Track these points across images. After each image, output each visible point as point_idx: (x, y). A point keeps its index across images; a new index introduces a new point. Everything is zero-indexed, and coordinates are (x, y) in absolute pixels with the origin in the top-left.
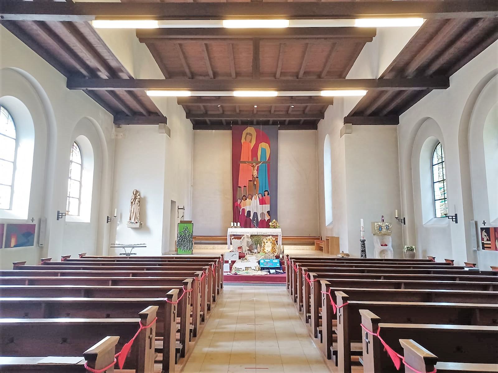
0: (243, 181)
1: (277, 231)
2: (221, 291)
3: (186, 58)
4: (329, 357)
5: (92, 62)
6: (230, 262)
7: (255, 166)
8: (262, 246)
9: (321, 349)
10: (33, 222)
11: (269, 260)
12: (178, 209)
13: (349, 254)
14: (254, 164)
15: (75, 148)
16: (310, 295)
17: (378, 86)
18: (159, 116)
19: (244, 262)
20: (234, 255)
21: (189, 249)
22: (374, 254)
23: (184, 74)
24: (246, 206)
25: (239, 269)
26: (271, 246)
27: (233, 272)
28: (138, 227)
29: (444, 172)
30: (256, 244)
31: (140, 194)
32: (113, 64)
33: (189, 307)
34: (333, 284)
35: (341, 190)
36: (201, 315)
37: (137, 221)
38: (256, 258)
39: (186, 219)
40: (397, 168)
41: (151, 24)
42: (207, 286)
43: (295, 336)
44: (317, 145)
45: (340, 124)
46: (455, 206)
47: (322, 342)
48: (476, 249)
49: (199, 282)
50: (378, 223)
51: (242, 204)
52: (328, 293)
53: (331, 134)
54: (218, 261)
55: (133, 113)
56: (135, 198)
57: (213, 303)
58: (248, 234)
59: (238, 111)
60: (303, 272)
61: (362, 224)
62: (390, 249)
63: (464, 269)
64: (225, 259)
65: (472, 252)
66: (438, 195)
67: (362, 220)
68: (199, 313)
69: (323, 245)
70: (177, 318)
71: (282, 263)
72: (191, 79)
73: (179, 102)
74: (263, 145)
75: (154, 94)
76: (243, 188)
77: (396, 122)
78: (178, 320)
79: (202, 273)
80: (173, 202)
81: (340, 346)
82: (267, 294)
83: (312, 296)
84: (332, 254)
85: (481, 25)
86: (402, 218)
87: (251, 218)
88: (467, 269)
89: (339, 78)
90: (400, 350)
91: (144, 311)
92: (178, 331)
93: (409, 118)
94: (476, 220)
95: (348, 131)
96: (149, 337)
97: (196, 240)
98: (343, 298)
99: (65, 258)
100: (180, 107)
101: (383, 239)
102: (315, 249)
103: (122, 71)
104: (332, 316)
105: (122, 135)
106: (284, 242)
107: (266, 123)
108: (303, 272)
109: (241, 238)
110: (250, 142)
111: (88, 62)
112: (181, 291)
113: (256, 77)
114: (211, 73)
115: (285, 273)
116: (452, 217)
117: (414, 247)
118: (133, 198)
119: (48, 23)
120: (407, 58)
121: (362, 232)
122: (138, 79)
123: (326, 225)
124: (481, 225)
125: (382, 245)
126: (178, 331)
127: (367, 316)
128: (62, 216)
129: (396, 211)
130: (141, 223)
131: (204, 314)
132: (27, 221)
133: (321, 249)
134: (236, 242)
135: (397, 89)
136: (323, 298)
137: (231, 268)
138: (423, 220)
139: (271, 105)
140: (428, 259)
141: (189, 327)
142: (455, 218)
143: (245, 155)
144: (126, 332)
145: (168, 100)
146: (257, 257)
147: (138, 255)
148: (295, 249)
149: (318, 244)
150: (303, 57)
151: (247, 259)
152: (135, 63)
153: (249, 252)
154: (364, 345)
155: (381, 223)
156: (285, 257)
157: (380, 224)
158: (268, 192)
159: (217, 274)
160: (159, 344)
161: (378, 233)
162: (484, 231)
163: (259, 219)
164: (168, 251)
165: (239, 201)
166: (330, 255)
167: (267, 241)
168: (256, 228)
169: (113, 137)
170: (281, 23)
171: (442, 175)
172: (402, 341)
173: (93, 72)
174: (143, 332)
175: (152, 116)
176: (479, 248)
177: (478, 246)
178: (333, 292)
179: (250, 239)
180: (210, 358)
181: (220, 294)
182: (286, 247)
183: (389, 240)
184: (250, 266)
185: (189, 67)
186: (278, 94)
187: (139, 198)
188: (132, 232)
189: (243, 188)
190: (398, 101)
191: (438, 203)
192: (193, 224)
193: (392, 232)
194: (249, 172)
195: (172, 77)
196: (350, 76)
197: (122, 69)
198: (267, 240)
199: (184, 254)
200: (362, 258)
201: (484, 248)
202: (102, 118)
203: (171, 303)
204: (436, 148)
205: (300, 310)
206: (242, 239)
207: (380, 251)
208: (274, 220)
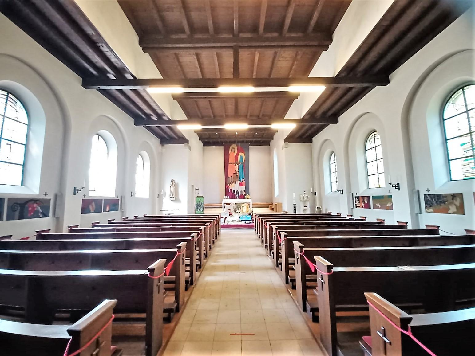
0: (230, 174)
1: (249, 201)
4: (278, 266)
5: (148, 111)
6: (224, 218)
9: (273, 262)
10: (85, 197)
16: (273, 240)
17: (302, 123)
22: (300, 211)
23: (198, 117)
25: (229, 221)
27: (226, 222)
30: (238, 208)
32: (118, 65)
33: (203, 242)
34: (279, 228)
35: (285, 178)
36: (209, 246)
42: (212, 231)
43: (260, 255)
44: (270, 153)
45: (282, 142)
47: (273, 258)
54: (217, 218)
55: (169, 137)
56: (172, 184)
57: (216, 240)
60: (264, 222)
61: (294, 196)
64: (221, 216)
65: (350, 209)
67: (294, 194)
68: (208, 245)
69: (273, 207)
71: (252, 217)
72: (203, 119)
73: (195, 132)
75: (182, 128)
78: (197, 248)
79: (210, 224)
81: (283, 260)
83: (268, 234)
84: (278, 212)
85: (315, 127)
87: (235, 193)
88: (348, 218)
90: (314, 262)
91: (179, 245)
92: (198, 255)
93: (318, 139)
95: (287, 146)
96: (157, 285)
99: (136, 217)
100: (196, 135)
104: (278, 244)
106: (253, 206)
108: (264, 222)
112: (198, 233)
113: (237, 116)
114: (212, 116)
115: (254, 223)
117: (321, 207)
118: (171, 184)
119: (124, 90)
120: (316, 107)
125: (304, 207)
126: (198, 255)
127: (297, 244)
128: (78, 191)
132: (38, 195)
133: (272, 209)
136: (274, 236)
140: (328, 213)
141: (203, 252)
142: (342, 192)
143: (231, 159)
144: (169, 256)
150: (261, 107)
154: (295, 259)
156: (254, 214)
157: (304, 195)
160: (188, 262)
162: (356, 198)
165: (228, 184)
172: (316, 258)
174: (179, 255)
175: (181, 140)
178: (279, 232)
180: (214, 268)
183: (308, 204)
184: (235, 219)
185: (201, 113)
190: (312, 130)
195: (191, 117)
200: (294, 214)
202: (154, 141)
204: (332, 155)
205: (262, 242)
208: (248, 195)
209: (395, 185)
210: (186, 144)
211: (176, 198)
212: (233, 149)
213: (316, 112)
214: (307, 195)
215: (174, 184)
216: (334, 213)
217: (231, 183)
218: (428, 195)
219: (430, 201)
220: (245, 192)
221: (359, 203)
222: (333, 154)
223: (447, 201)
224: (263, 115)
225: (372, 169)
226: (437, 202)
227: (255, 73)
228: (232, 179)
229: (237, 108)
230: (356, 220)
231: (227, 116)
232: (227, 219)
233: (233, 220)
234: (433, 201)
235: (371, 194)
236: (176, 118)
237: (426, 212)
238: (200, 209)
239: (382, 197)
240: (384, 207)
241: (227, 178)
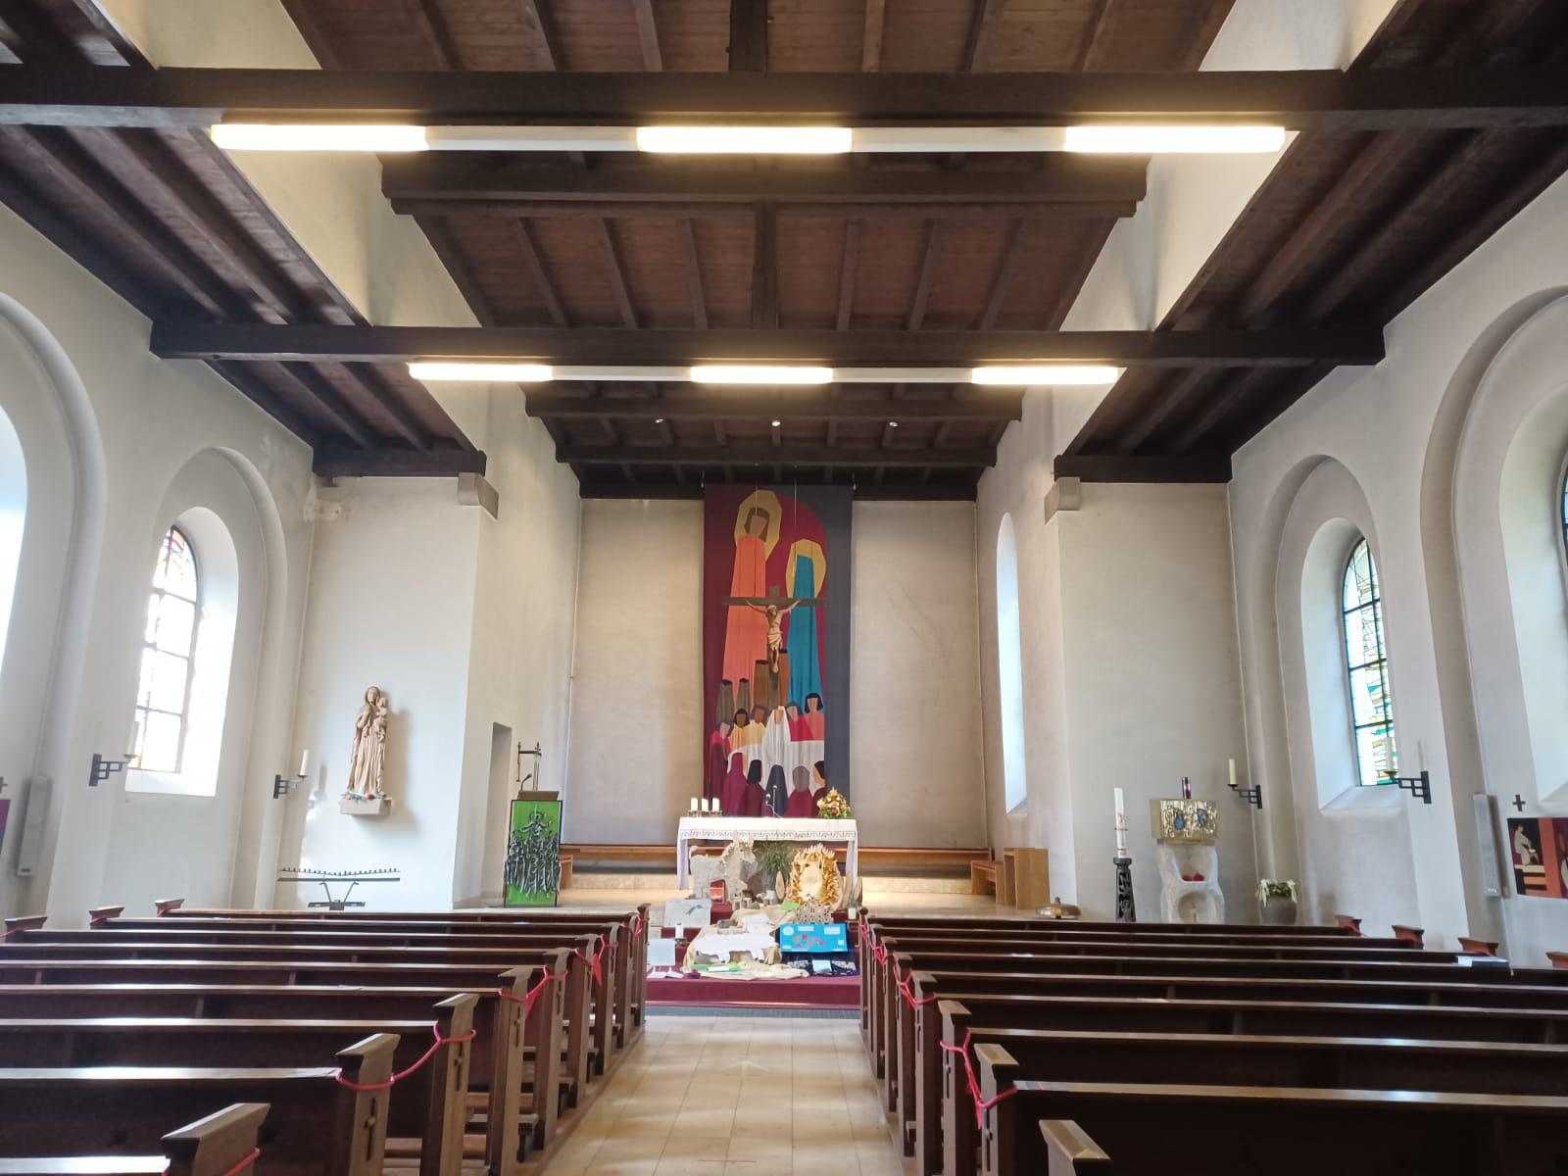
0: (737, 665)
1: (843, 829)
2: (632, 1034)
3: (547, 265)
5: (233, 270)
6: (679, 934)
7: (774, 613)
8: (792, 877)
11: (811, 928)
12: (520, 752)
13: (1079, 906)
14: (770, 607)
15: (178, 550)
18: (461, 448)
19: (728, 933)
20: (693, 909)
21: (545, 888)
22: (1160, 907)
23: (546, 320)
24: (748, 745)
25: (707, 960)
28: (377, 812)
29: (1381, 633)
31: (387, 702)
32: (301, 276)
35: (1057, 693)
37: (373, 792)
39: (545, 786)
41: (410, 138)
45: (1043, 481)
46: (1419, 745)
48: (1494, 891)
49: (515, 1006)
50: (1171, 803)
51: (733, 740)
52: (960, 1050)
53: (1018, 511)
54: (625, 935)
55: (366, 435)
56: (372, 716)
58: (745, 839)
59: (720, 438)
61: (1119, 808)
62: (1212, 891)
63: (1456, 961)
65: (1483, 904)
66: (1366, 709)
67: (1118, 793)
69: (997, 875)
70: (467, 1136)
71: (851, 939)
74: (805, 548)
76: (736, 685)
77: (1219, 471)
80: (500, 731)
88: (1465, 962)
89: (1039, 328)
93: (1266, 461)
94: (1492, 794)
95: (1072, 500)
97: (577, 859)
98: (1000, 1071)
99: (101, 918)
100: (535, 425)
101: (1189, 858)
103: (331, 301)
105: (340, 509)
107: (812, 477)
109: (723, 850)
110: (761, 537)
111: (221, 271)
114: (628, 314)
116: (1413, 784)
117: (1291, 884)
118: (366, 713)
119: (80, 136)
121: (1119, 833)
122: (383, 324)
123: (1008, 811)
125: (1186, 878)
128: (108, 771)
129: (1232, 763)
130: (387, 799)
131: (541, 1123)
134: (707, 867)
135: (1218, 363)
136: (946, 1067)
137: (680, 954)
139: (826, 418)
142: (1423, 787)
143: (747, 578)
145: (493, 393)
146: (771, 916)
147: (370, 908)
149: (982, 874)
151: (739, 924)
152: (345, 256)
153: (746, 899)
155: (1182, 803)
157: (1180, 805)
159: (611, 976)
161: (1173, 835)
162: (1521, 829)
163: (790, 788)
164: (476, 893)
165: (724, 728)
166: (997, 906)
168: (776, 817)
169: (310, 515)
170: (826, 140)
171: (1375, 644)
173: (237, 302)
175: (431, 446)
176: (1506, 890)
179: (753, 856)
181: (626, 1049)
182: (867, 881)
183: (1210, 861)
184: (746, 947)
185: (561, 298)
186: (834, 377)
187: (385, 716)
188: (356, 828)
189: (736, 685)
190: (1226, 403)
191: (1365, 737)
192: (562, 802)
193: (1218, 834)
194: (757, 636)
195: (501, 326)
196: (1074, 321)
197: (329, 291)
198: (807, 857)
199: (527, 906)
200: (1122, 921)
201: (1522, 888)
202: (269, 459)
203: (355, 1086)
204: (1352, 556)
206: (724, 854)
207: (1179, 897)
209: (1412, 780)
210: (472, 475)
211: (387, 803)
212: (755, 518)
213: (1246, 284)
214: (1201, 806)
215: (383, 721)
216: (1377, 927)
217: (741, 718)
220: (822, 776)
221: (1541, 863)
222: (1361, 552)
224: (930, 318)
227: (872, 40)
228: (744, 693)
229: (763, 251)
230: (1525, 976)
231: (715, 319)
232: (695, 945)
233: (732, 953)
236: (402, 318)
238: (532, 879)
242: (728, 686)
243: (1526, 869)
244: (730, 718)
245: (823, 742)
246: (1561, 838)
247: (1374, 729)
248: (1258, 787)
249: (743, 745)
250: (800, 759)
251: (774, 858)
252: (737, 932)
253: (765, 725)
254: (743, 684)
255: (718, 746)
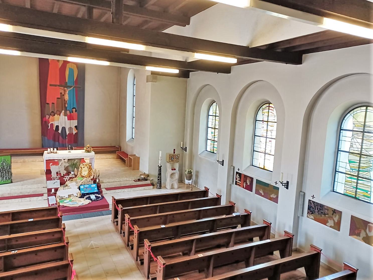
0: (51, 98)
9: (124, 241)
11: (88, 186)
21: (8, 179)
26: (87, 170)
38: (76, 184)
40: (185, 111)
61: (160, 155)
65: (229, 185)
66: (210, 136)
67: (160, 152)
82: (99, 232)
86: (184, 147)
87: (60, 131)
102: (116, 158)
121: (160, 161)
123: (127, 141)
124: (236, 170)
125: (172, 170)
138: (199, 152)
148: (100, 158)
151: (68, 186)
158: (76, 109)
162: (238, 174)
165: (47, 117)
167: (83, 166)
177: (233, 182)
201: (236, 184)
217: (53, 114)
218: (313, 201)
219: (313, 208)
220: (77, 130)
221: (240, 181)
222: (215, 104)
223: (328, 214)
225: (260, 144)
226: (319, 211)
234: (316, 209)
235: (256, 175)
237: (308, 217)
238: (3, 177)
239: (267, 185)
240: (266, 196)
241: (45, 107)
242: (48, 105)
243: (237, 181)
244: (49, 114)
245: (77, 121)
246: (245, 178)
247: (212, 141)
248: (186, 147)
249: (53, 121)
250: (70, 125)
251: (74, 164)
252: (69, 188)
253: (60, 116)
254: (53, 104)
255: (45, 122)
